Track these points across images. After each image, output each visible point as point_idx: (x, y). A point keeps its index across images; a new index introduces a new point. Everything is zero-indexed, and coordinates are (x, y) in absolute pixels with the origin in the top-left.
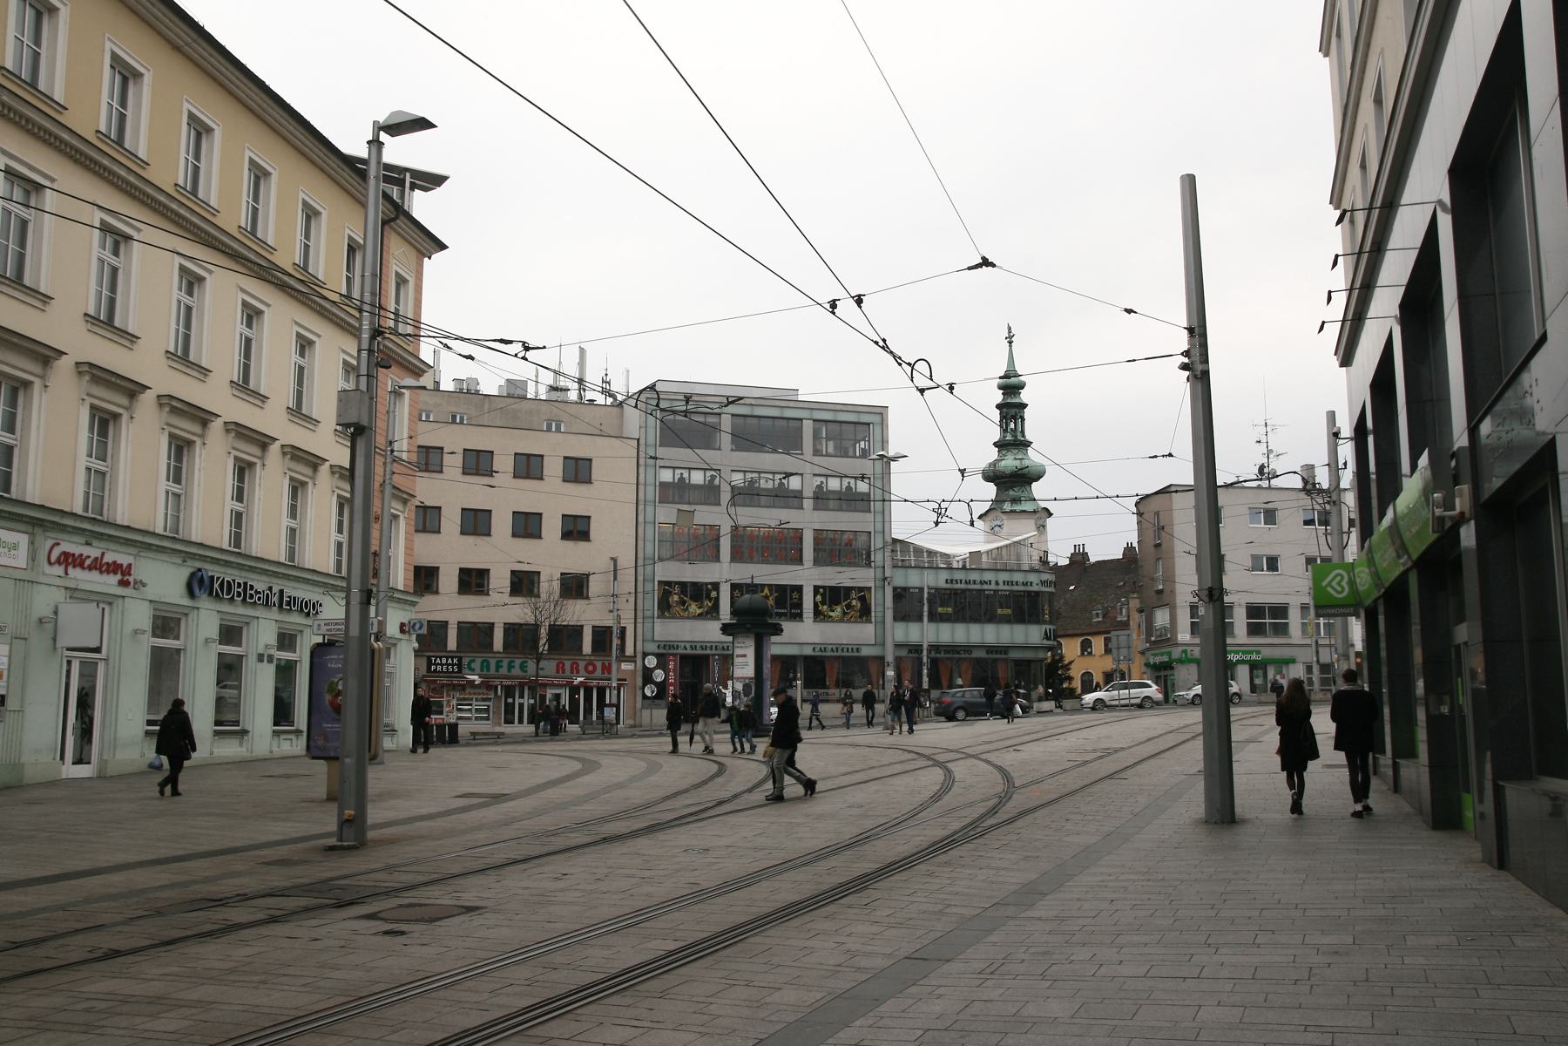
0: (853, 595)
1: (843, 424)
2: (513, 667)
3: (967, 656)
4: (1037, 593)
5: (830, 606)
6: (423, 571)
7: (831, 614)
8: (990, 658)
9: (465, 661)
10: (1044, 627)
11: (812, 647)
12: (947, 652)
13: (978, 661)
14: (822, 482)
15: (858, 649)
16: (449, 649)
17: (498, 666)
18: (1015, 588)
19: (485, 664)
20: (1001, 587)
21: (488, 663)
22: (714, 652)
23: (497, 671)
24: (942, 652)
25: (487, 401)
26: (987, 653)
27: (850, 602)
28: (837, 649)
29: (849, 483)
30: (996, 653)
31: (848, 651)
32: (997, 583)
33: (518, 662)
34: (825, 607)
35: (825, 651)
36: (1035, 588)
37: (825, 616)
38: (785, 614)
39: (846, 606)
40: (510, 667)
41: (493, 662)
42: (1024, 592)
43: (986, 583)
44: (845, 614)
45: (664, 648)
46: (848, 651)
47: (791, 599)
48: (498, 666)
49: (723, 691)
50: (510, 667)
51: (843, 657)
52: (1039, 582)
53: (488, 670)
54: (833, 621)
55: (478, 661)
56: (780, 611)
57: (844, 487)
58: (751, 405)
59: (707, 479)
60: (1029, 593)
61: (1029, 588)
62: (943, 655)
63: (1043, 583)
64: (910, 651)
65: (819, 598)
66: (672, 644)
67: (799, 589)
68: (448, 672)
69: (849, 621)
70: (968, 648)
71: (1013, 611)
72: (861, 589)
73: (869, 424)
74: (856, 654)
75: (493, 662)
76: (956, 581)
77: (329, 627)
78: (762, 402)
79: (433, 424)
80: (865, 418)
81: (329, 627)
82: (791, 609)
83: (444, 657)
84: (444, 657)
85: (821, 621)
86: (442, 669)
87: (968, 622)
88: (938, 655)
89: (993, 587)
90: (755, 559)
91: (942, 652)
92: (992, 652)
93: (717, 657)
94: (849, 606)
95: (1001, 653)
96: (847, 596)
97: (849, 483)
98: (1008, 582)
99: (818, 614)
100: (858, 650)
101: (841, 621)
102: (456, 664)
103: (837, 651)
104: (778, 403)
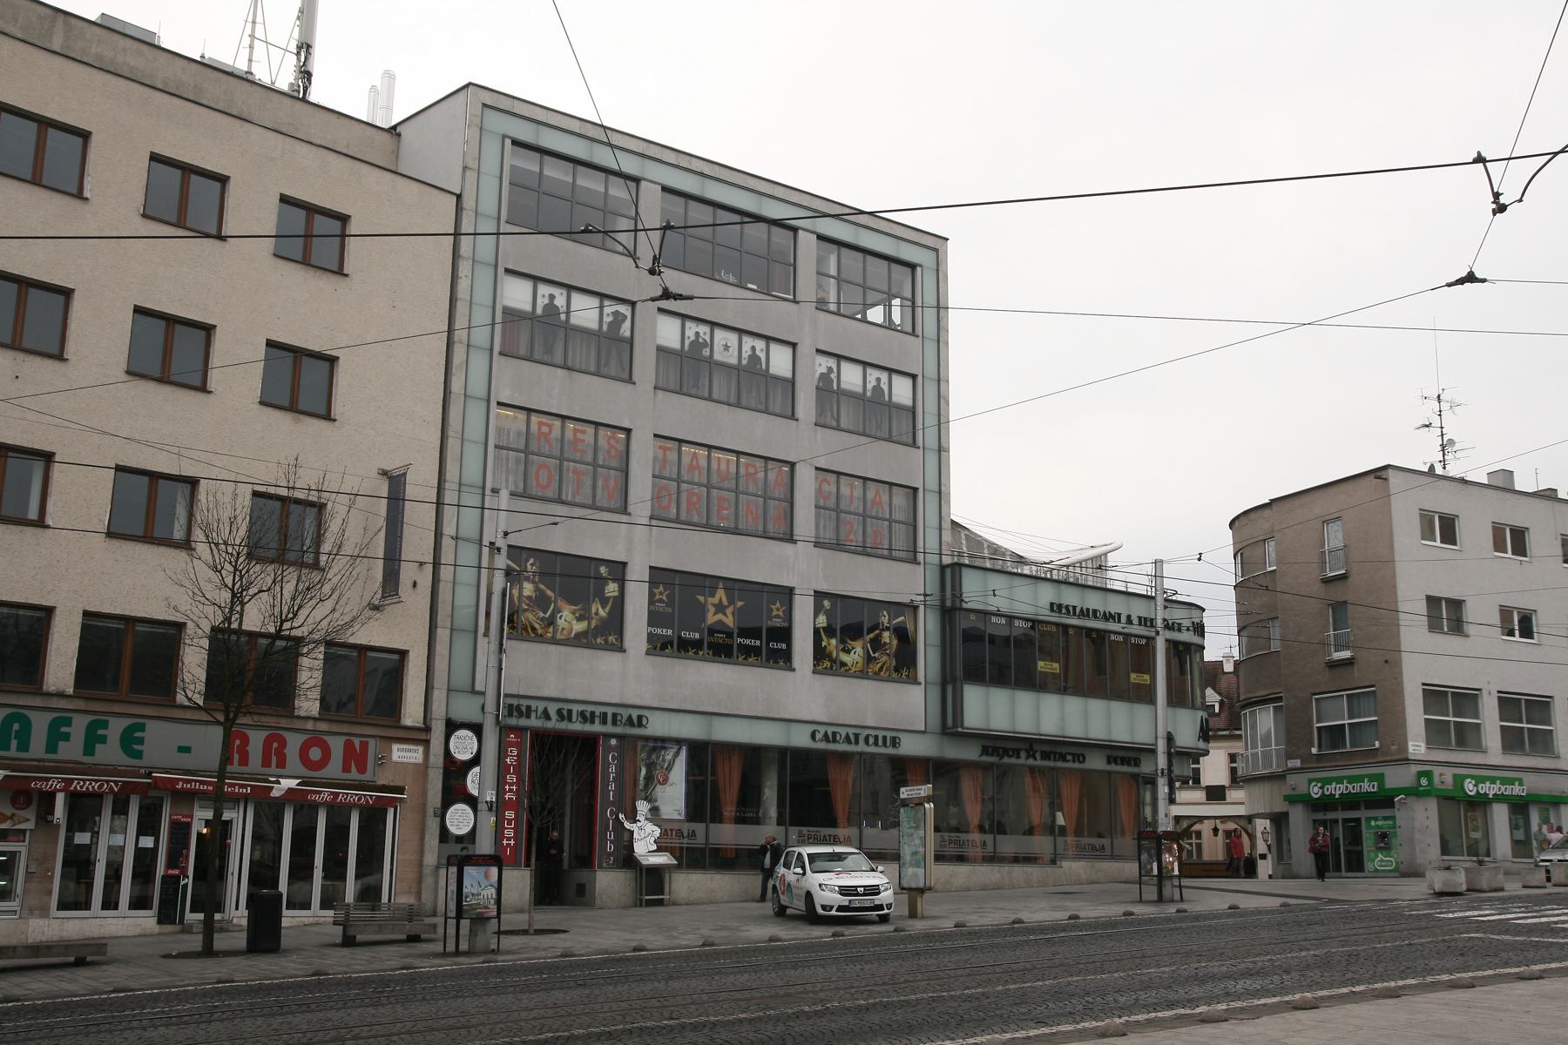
7: (844, 657)
14: (830, 370)
17: (56, 735)
19: (275, 745)
21: (283, 743)
22: (609, 728)
23: (52, 747)
27: (880, 635)
28: (857, 736)
33: (116, 727)
34: (834, 642)
35: (835, 741)
40: (93, 739)
44: (869, 660)
48: (56, 735)
49: (627, 825)
50: (93, 739)
51: (861, 754)
54: (847, 674)
69: (876, 677)
74: (890, 751)
78: (779, 193)
85: (826, 672)
91: (1038, 755)
93: (613, 742)
94: (877, 644)
97: (878, 380)
100: (895, 742)
101: (862, 674)
103: (857, 742)
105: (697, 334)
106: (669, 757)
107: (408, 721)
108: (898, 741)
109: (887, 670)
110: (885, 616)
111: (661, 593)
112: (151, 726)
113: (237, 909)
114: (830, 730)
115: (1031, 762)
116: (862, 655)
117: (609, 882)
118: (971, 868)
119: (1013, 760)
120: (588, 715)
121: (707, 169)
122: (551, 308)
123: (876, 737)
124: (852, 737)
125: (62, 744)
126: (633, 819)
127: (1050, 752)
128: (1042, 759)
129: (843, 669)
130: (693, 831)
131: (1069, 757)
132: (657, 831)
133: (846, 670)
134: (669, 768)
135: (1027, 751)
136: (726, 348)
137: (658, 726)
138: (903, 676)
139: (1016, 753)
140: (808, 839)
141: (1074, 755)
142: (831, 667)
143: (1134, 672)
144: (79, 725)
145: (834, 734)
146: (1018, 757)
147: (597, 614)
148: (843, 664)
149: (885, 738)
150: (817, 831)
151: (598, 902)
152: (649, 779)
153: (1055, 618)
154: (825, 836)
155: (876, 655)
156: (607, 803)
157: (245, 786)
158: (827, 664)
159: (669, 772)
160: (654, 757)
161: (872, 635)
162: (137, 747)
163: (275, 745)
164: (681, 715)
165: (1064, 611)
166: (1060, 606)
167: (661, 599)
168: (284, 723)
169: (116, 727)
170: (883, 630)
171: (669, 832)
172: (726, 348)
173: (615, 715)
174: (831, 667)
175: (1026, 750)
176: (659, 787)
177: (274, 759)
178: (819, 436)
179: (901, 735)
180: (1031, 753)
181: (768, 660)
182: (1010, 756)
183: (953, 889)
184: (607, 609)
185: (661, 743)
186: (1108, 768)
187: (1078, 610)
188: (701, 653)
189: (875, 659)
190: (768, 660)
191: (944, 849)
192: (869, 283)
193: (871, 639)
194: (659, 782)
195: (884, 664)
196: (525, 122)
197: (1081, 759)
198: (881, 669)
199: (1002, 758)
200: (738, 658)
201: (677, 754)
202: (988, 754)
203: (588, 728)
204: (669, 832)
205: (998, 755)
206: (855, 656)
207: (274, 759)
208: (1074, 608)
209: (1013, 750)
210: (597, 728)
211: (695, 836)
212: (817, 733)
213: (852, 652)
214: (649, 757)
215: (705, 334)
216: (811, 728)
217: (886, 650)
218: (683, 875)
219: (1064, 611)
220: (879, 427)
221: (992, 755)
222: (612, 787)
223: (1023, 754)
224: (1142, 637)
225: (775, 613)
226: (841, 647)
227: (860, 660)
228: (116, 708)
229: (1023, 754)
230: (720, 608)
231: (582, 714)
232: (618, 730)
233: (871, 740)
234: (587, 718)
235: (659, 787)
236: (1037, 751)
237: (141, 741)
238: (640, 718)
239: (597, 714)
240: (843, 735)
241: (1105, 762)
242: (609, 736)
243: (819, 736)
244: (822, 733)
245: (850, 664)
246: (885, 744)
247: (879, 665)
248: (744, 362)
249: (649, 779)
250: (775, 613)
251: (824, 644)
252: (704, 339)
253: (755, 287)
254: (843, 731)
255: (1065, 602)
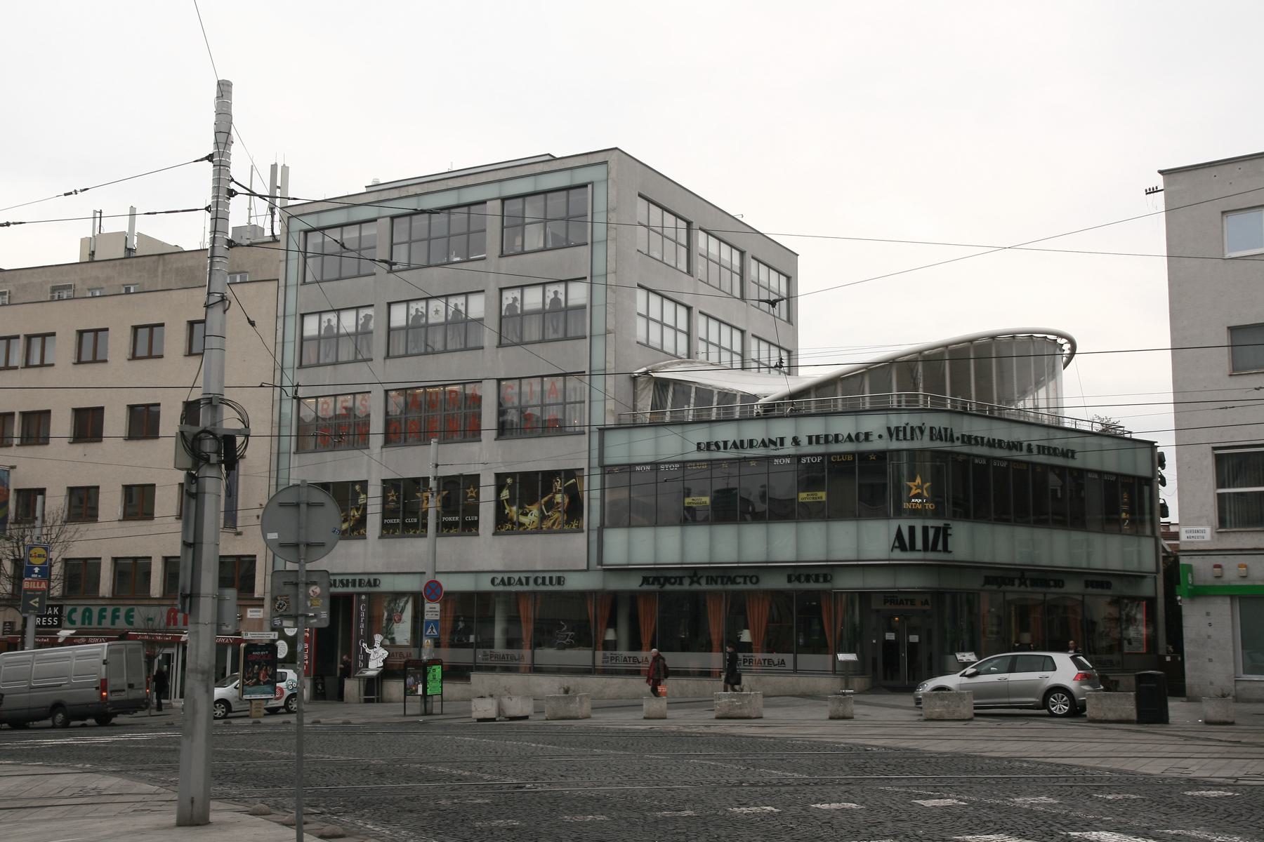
0: (558, 485)
1: (550, 195)
2: (105, 617)
3: (749, 586)
4: (882, 455)
5: (521, 507)
6: (540, 474)
7: (523, 519)
8: (797, 591)
9: (66, 610)
10: (894, 524)
11: (489, 577)
12: (711, 580)
13: (776, 594)
14: (515, 299)
15: (559, 578)
16: (101, 595)
17: (101, 617)
18: (835, 448)
19: (87, 614)
20: (806, 448)
21: (91, 612)
22: (358, 589)
23: (100, 623)
24: (703, 581)
25: (161, 261)
26: (790, 581)
27: (553, 497)
28: (527, 579)
29: (556, 293)
30: (808, 579)
31: (544, 583)
32: (796, 441)
33: (123, 610)
34: (514, 508)
35: (509, 584)
36: (876, 445)
37: (513, 523)
38: (455, 524)
39: (546, 504)
40: (115, 617)
41: (96, 611)
42: (853, 454)
43: (774, 443)
44: (543, 518)
45: (354, 585)
46: (551, 582)
47: (466, 498)
48: (101, 617)
49: (367, 650)
50: (115, 617)
51: (534, 593)
52: (885, 434)
53: (90, 623)
54: (526, 532)
55: (80, 610)
56: (450, 519)
57: (548, 301)
58: (416, 195)
59: (360, 322)
60: (863, 456)
61: (865, 447)
62: (704, 586)
63: (893, 433)
64: (646, 580)
65: (505, 494)
66: (357, 578)
67: (474, 480)
68: (47, 626)
69: (550, 531)
70: (754, 572)
71: (712, 502)
72: (570, 473)
73: (585, 186)
74: (557, 588)
75: (96, 611)
76: (717, 444)
77: (1189, 535)
78: (470, 180)
79: (134, 295)
80: (581, 177)
81: (1189, 535)
82: (404, 519)
83: (56, 606)
84: (56, 606)
85: (510, 532)
86: (41, 622)
87: (798, 522)
88: (695, 587)
89: (789, 449)
90: (410, 440)
91: (703, 581)
92: (798, 579)
93: (363, 597)
94: (550, 505)
95: (817, 581)
96: (548, 489)
97: (556, 293)
98: (818, 437)
99: (503, 523)
100: (375, 583)
101: (538, 530)
102: (56, 616)
103: (527, 583)
104: (451, 184)
105: (417, 310)
106: (402, 604)
107: (256, 595)
108: (562, 579)
109: (559, 524)
110: (557, 481)
111: (472, 492)
112: (136, 608)
113: (175, 697)
114: (506, 576)
115: (1023, 588)
116: (537, 515)
117: (352, 687)
118: (624, 680)
119: (677, 587)
120: (345, 582)
121: (418, 190)
122: (556, 300)
123: (544, 578)
124: (524, 581)
125: (103, 621)
126: (371, 646)
127: (717, 577)
128: (707, 583)
129: (521, 529)
130: (783, 660)
131: (1052, 583)
132: (386, 654)
133: (525, 529)
134: (402, 612)
135: (1020, 579)
136: (437, 312)
137: (387, 585)
138: (574, 527)
139: (680, 580)
140: (491, 657)
141: (745, 577)
142: (512, 529)
143: (804, 491)
144: (110, 610)
145: (509, 579)
146: (1013, 585)
147: (353, 516)
148: (521, 524)
149: (551, 578)
150: (752, 656)
151: (345, 699)
152: (390, 620)
153: (704, 455)
154: (625, 658)
155: (550, 513)
156: (359, 637)
157: (168, 636)
158: (509, 526)
159: (402, 614)
160: (392, 605)
161: (546, 499)
162: (132, 620)
163: (87, 614)
164: (401, 576)
165: (973, 442)
166: (969, 437)
167: (472, 496)
168: (92, 602)
169: (123, 610)
170: (556, 493)
171: (628, 659)
172: (437, 312)
173: (360, 580)
174: (512, 529)
175: (690, 577)
176: (395, 624)
177: (87, 621)
178: (500, 355)
179: (566, 575)
180: (1023, 580)
181: (463, 530)
182: (1006, 585)
183: (606, 697)
184: (360, 513)
185: (397, 595)
186: (789, 586)
187: (986, 440)
188: (418, 532)
189: (549, 516)
190: (463, 530)
191: (606, 665)
192: (465, 230)
193: (545, 502)
194: (395, 620)
195: (556, 519)
196: (561, 173)
197: (1061, 584)
198: (553, 524)
199: (663, 585)
200: (442, 531)
201: (406, 602)
202: (648, 584)
203: (345, 590)
204: (628, 659)
205: (659, 583)
206: (532, 517)
207: (87, 621)
208: (982, 438)
209: (675, 578)
210: (350, 589)
211: (784, 664)
212: (496, 580)
213: (530, 514)
214: (389, 604)
215: (422, 307)
216: (491, 576)
217: (559, 508)
218: (396, 683)
219: (973, 442)
220: (555, 331)
221: (653, 584)
222: (362, 626)
223: (1017, 582)
224: (817, 455)
225: (469, 495)
226: (520, 511)
227: (536, 519)
228: (121, 602)
229: (1017, 582)
230: (393, 496)
231: (341, 581)
232: (365, 589)
233: (540, 581)
234: (345, 584)
235: (395, 624)
236: (702, 577)
237: (132, 617)
238: (375, 580)
239: (350, 581)
240: (517, 579)
241: (786, 580)
242: (359, 594)
243: (497, 581)
244: (500, 579)
245: (527, 524)
246: (551, 582)
247: (552, 521)
248: (547, 307)
249: (390, 620)
250: (469, 495)
251: (506, 511)
252: (421, 312)
253: (458, 259)
254: (516, 576)
255: (746, 438)
